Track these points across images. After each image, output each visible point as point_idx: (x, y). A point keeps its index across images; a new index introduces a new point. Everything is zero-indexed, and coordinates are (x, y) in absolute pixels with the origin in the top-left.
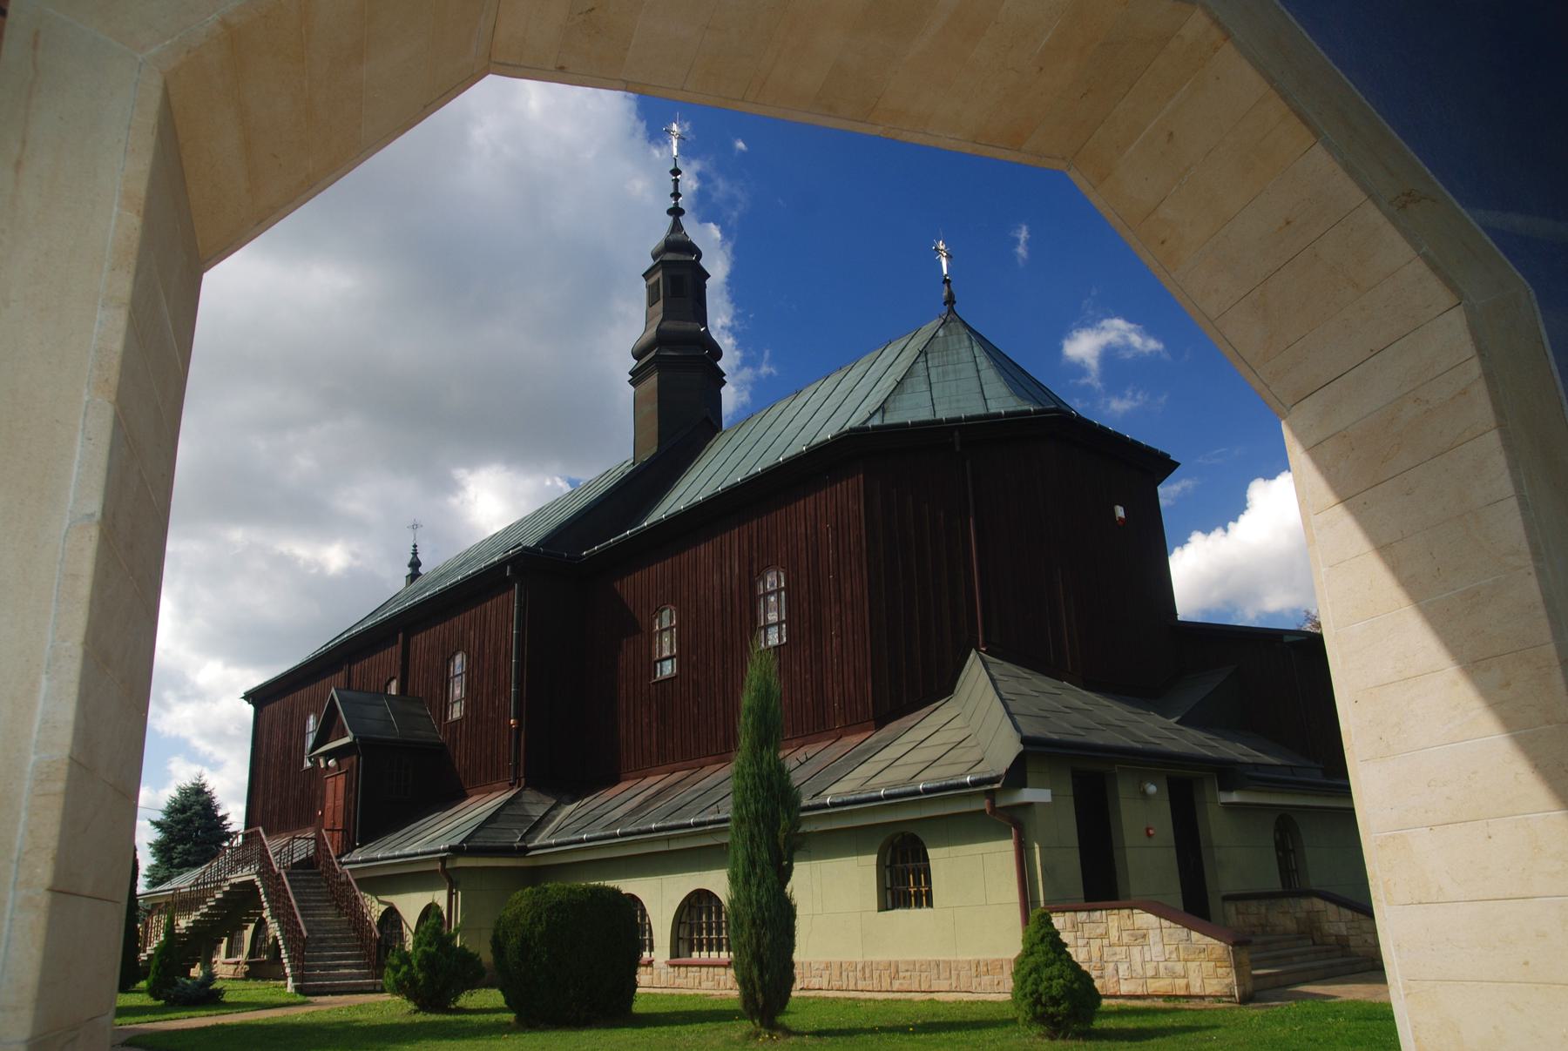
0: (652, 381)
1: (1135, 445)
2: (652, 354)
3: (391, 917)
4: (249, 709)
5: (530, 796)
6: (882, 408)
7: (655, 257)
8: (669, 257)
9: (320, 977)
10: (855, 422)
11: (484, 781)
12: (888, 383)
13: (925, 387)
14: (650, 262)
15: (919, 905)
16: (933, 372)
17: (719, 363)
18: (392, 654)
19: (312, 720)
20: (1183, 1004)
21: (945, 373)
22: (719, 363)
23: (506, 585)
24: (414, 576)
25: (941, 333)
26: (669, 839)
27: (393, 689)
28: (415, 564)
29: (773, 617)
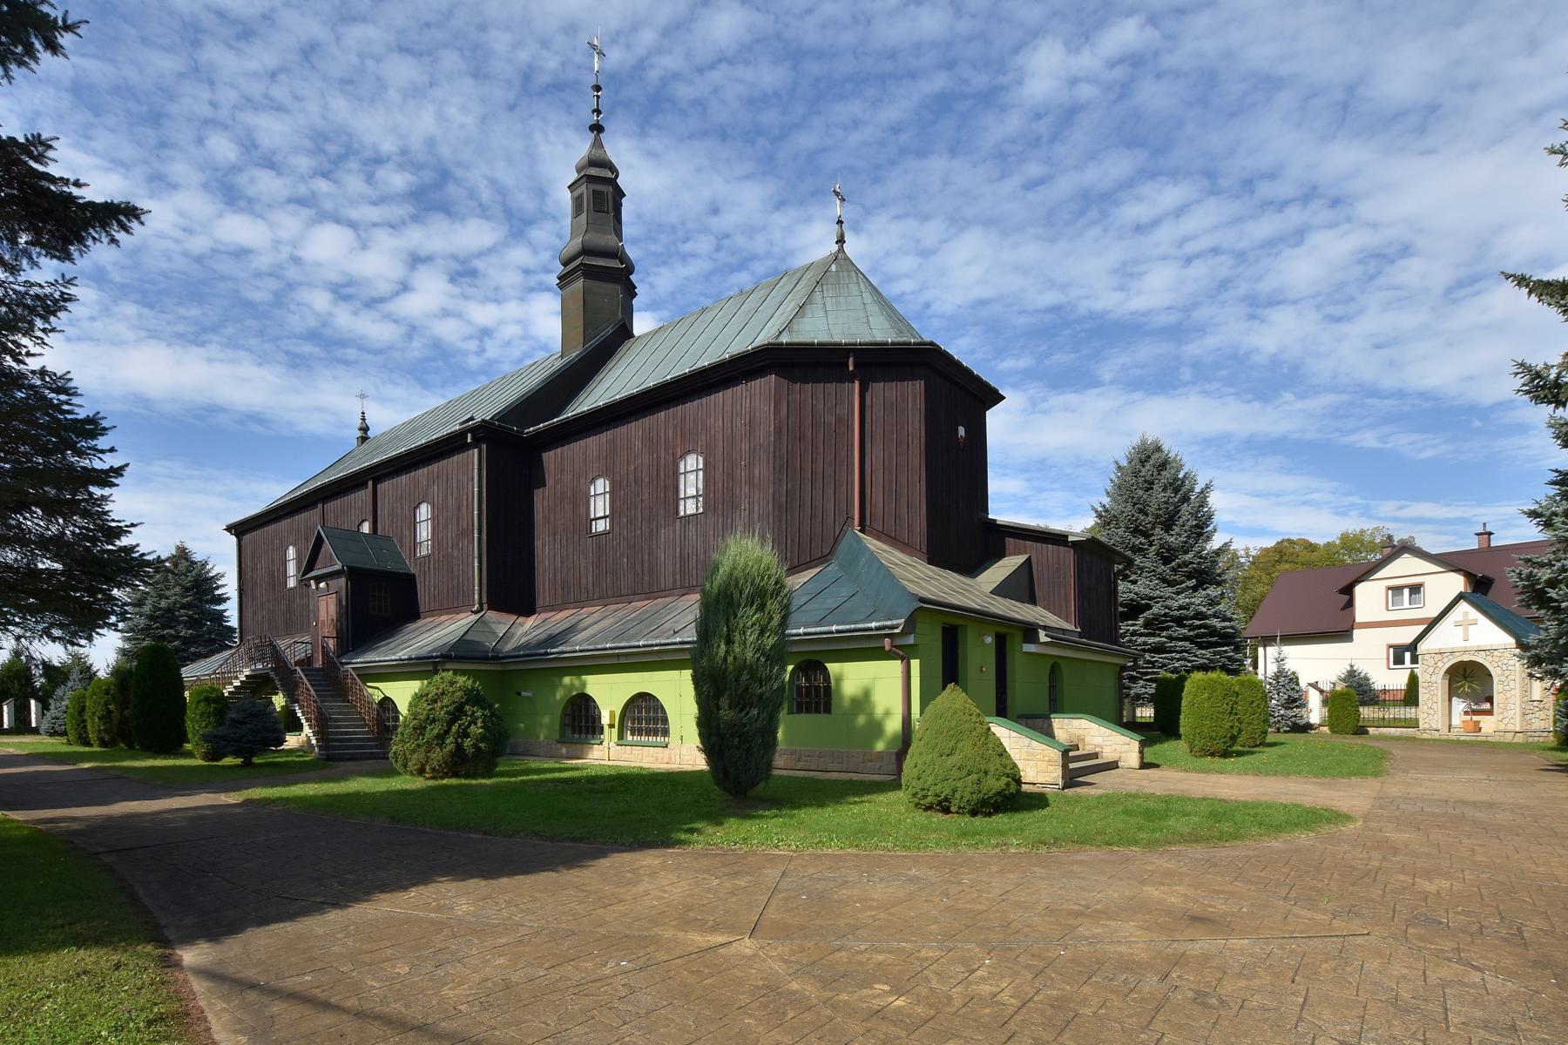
0: (579, 284)
1: (978, 379)
2: (578, 262)
3: (387, 703)
4: (232, 540)
5: (492, 615)
6: (788, 326)
7: (578, 171)
8: (593, 171)
9: (339, 748)
10: (762, 339)
11: (452, 606)
12: (790, 307)
13: (822, 314)
14: (574, 176)
15: (817, 711)
16: (828, 301)
17: (632, 277)
18: (364, 495)
19: (291, 552)
20: (1470, 812)
21: (838, 304)
22: (632, 277)
23: (466, 447)
24: (364, 439)
25: (833, 268)
26: (618, 655)
27: (366, 528)
28: (365, 429)
29: (691, 491)
